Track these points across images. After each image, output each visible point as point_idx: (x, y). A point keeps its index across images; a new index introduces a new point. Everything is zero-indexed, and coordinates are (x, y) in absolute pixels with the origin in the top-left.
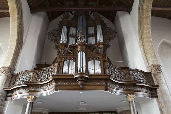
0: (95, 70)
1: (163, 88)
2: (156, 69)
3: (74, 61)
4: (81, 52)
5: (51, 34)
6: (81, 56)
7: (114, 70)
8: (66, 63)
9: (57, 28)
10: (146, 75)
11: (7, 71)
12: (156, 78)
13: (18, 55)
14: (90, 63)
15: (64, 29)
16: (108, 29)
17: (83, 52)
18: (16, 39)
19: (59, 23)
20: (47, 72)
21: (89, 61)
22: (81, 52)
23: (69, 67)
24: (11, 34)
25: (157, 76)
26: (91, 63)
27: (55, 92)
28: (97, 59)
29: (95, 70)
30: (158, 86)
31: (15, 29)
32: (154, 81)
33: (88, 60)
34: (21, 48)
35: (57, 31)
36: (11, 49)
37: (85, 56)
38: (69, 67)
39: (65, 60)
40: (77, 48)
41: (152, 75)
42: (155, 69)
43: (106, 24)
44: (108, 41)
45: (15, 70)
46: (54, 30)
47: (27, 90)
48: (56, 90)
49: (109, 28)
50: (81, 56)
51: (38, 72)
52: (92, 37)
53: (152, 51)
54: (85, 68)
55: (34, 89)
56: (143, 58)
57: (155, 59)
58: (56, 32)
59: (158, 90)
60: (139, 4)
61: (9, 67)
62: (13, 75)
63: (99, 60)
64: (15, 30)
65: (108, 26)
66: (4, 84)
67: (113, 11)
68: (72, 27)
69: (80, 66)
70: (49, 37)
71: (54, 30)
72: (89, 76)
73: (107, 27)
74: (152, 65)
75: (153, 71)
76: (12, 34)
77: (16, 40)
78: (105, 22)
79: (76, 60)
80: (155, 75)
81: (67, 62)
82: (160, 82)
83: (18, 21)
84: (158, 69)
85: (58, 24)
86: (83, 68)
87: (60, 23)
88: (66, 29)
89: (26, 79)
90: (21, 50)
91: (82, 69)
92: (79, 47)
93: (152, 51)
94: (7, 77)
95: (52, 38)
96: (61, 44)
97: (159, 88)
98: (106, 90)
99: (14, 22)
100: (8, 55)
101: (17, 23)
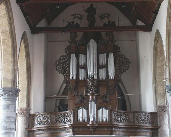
0: (103, 118)
1: (163, 128)
2: (161, 110)
3: (86, 109)
4: (92, 102)
5: (59, 63)
6: (92, 105)
7: (121, 114)
8: (80, 112)
9: (65, 54)
10: (152, 115)
11: (25, 112)
12: (159, 119)
13: (30, 93)
14: (99, 111)
15: (73, 58)
16: (121, 57)
17: (94, 40)
18: (26, 77)
19: (66, 48)
20: (63, 116)
21: (99, 109)
22: (92, 102)
23: (82, 115)
24: (20, 71)
25: (161, 117)
26: (100, 111)
27: (73, 136)
28: (105, 108)
29: (103, 118)
30: (160, 127)
31: (23, 66)
32: (158, 121)
33: (98, 108)
34: (31, 84)
35: (64, 59)
36: (22, 88)
37: (95, 105)
38: (82, 115)
39: (79, 109)
40: (89, 97)
41: (158, 115)
42: (160, 110)
43: (119, 49)
44: (120, 73)
45: (30, 109)
46: (61, 58)
47: (48, 132)
48: (74, 134)
49: (123, 55)
50: (92, 105)
51: (55, 115)
52: (103, 69)
53: (162, 90)
54: (95, 117)
55: (55, 131)
56: (153, 95)
57: (163, 99)
58: (64, 61)
59: (159, 129)
60: (155, 37)
61: (26, 109)
62: (30, 115)
63: (107, 109)
64: (24, 67)
65: (122, 53)
66: (25, 124)
67: (138, 2)
68: (82, 54)
69: (91, 116)
70: (57, 68)
71: (61, 57)
72: (98, 125)
73: (121, 55)
74: (159, 106)
75: (159, 111)
76: (21, 72)
77: (26, 78)
78: (118, 47)
79: (87, 108)
80: (159, 116)
81: (81, 110)
82: (162, 123)
83: (26, 58)
84: (163, 110)
85: (65, 49)
86: (94, 75)
87: (67, 48)
88: (75, 57)
89: (45, 121)
90: (31, 86)
91: (93, 118)
92: (90, 97)
93: (162, 90)
94: (26, 118)
95: (61, 70)
96: (71, 80)
97: (161, 128)
98: (111, 134)
99: (22, 60)
100: (22, 95)
101: (25, 61)
